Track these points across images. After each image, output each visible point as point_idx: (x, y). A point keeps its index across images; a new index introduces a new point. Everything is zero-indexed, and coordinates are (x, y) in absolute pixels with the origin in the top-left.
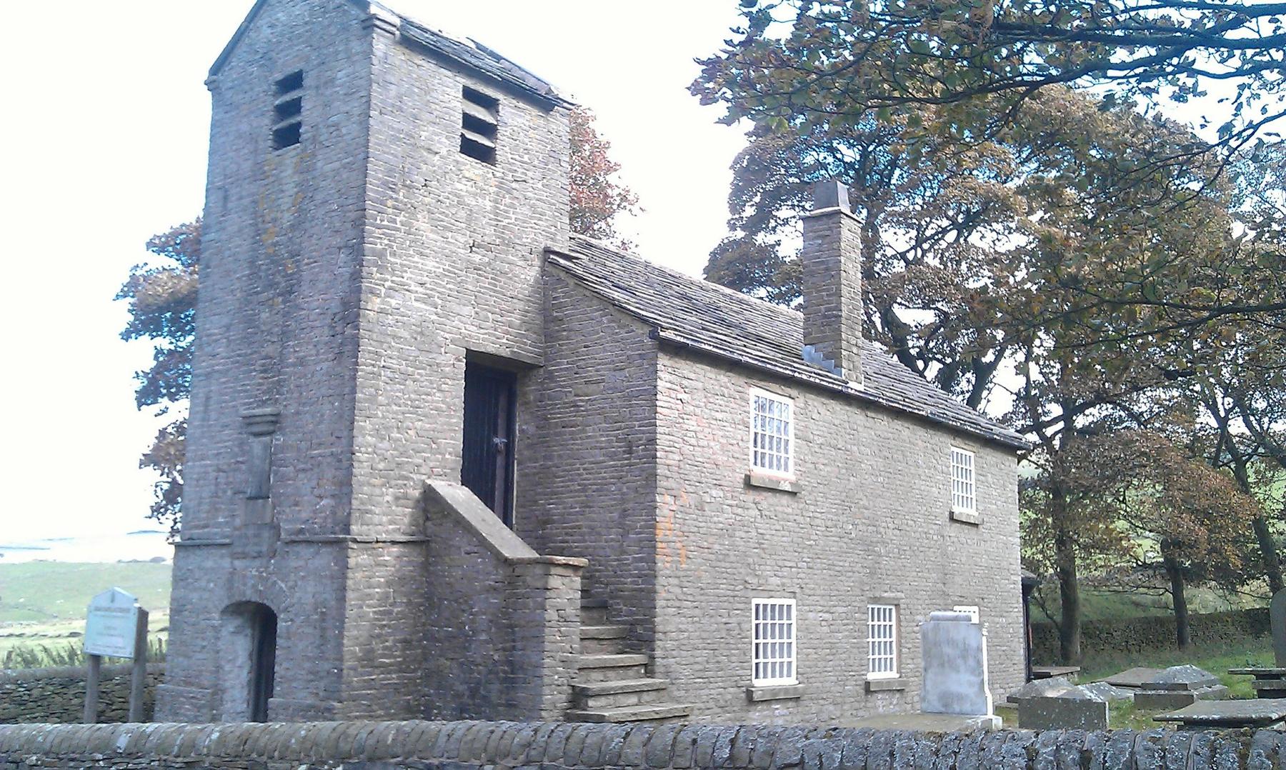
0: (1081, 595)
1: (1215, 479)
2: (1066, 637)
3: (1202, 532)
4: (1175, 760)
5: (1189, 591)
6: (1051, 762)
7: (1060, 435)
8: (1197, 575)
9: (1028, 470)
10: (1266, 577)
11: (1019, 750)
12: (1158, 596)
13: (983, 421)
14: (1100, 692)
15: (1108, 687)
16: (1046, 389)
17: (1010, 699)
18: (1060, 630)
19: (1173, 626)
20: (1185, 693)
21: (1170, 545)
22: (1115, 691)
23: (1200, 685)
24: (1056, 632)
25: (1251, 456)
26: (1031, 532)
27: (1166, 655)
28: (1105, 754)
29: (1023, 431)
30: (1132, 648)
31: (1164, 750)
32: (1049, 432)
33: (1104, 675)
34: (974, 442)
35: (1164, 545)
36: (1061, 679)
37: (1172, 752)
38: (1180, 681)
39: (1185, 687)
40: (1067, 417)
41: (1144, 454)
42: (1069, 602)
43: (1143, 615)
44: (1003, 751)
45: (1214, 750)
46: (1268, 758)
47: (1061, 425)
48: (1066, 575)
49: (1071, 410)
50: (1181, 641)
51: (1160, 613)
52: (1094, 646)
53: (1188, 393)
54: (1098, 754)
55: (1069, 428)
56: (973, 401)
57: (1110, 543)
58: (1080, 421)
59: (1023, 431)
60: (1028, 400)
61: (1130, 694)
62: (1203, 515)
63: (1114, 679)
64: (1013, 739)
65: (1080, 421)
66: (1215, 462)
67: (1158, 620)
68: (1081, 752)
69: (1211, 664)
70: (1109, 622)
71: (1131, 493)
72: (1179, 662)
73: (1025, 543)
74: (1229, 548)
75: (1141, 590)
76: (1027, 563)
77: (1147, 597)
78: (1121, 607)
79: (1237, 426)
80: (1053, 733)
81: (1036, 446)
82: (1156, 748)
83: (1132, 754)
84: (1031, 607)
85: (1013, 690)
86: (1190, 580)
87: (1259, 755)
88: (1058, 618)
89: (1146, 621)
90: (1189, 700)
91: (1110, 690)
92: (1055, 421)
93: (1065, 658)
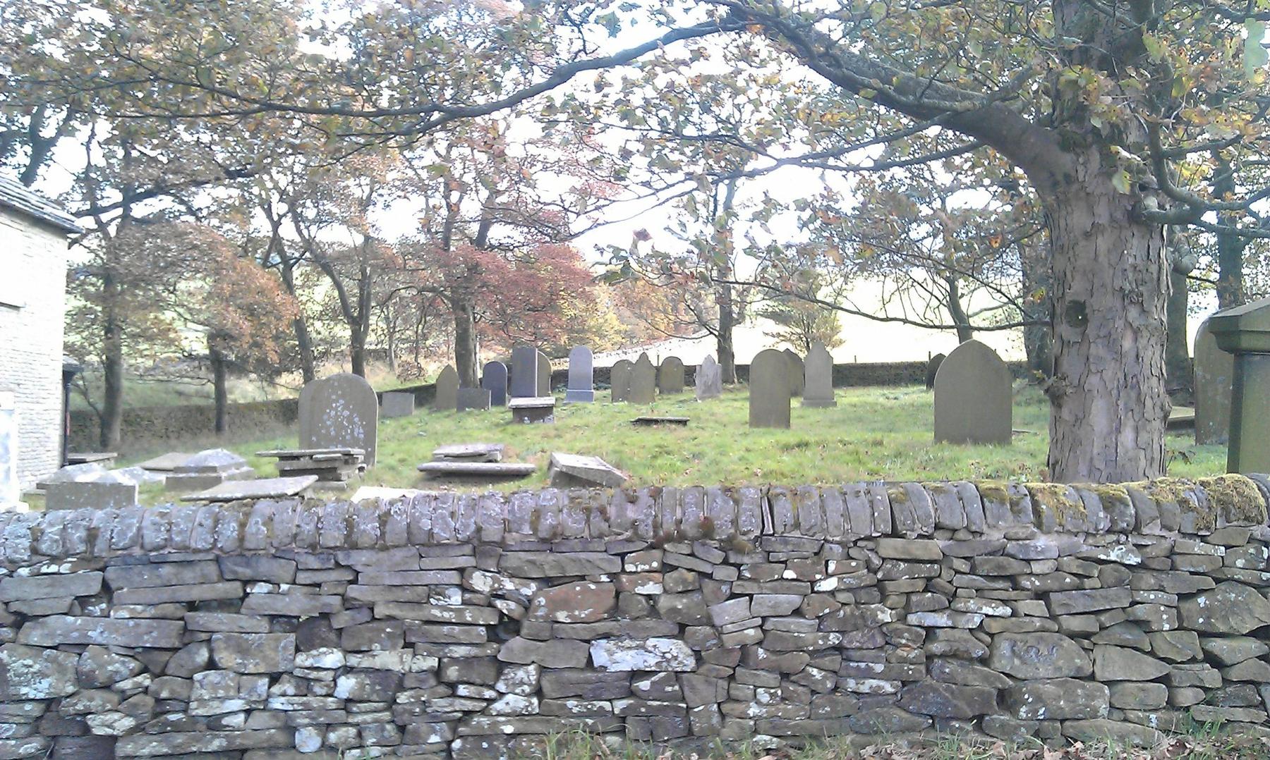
0: (125, 384)
1: (264, 279)
2: (106, 421)
3: (246, 326)
4: (181, 532)
5: (230, 382)
6: (56, 541)
7: (119, 220)
8: (240, 368)
9: (80, 256)
10: (301, 371)
11: (24, 531)
12: (200, 387)
13: (34, 199)
14: (133, 476)
15: (140, 471)
16: (107, 175)
17: (40, 486)
18: (101, 418)
19: (212, 415)
20: (214, 475)
21: (218, 336)
22: (148, 476)
23: (225, 468)
24: (96, 420)
25: (298, 260)
26: (77, 320)
27: (202, 440)
28: (112, 530)
29: (78, 214)
30: (171, 435)
31: (170, 524)
32: (105, 217)
33: (138, 461)
34: (22, 220)
35: (211, 337)
36: (95, 464)
37: (177, 525)
38: (211, 464)
39: (214, 469)
40: (126, 204)
41: (195, 247)
42: (112, 390)
43: (185, 403)
44: (6, 533)
45: (217, 522)
46: (264, 524)
47: (119, 211)
48: (111, 365)
49: (131, 197)
50: (219, 428)
51: (197, 401)
52: (134, 432)
53: (246, 194)
54: (106, 530)
55: (126, 216)
56: (28, 177)
57: (163, 334)
58: (140, 210)
59: (78, 214)
60: (88, 181)
61: (162, 477)
62: (250, 312)
63: (150, 463)
64: (19, 520)
65: (140, 210)
66: (266, 263)
67: (200, 410)
68: (89, 529)
69: (243, 448)
70: (150, 410)
71: (182, 285)
72: (214, 446)
73: (68, 329)
74: (270, 344)
75: (186, 380)
76: (69, 349)
77: (190, 386)
78: (164, 395)
79: (288, 231)
80: (61, 512)
81: (90, 231)
82: (163, 522)
83: (139, 529)
84: (72, 395)
85: (45, 477)
86: (232, 373)
87: (257, 523)
88: (101, 406)
89: (188, 409)
90: (218, 481)
91: (143, 474)
92: (115, 206)
93: (104, 445)
